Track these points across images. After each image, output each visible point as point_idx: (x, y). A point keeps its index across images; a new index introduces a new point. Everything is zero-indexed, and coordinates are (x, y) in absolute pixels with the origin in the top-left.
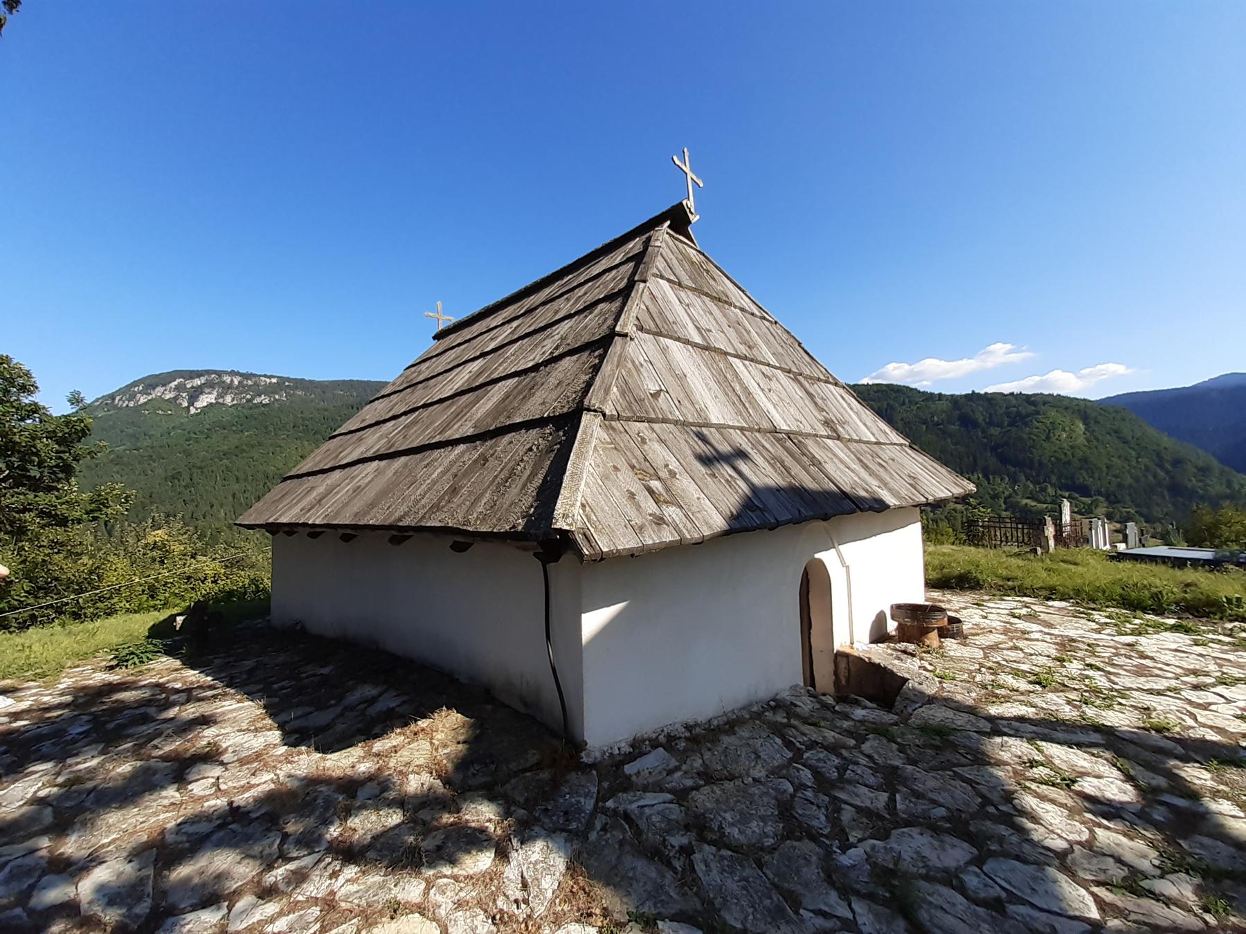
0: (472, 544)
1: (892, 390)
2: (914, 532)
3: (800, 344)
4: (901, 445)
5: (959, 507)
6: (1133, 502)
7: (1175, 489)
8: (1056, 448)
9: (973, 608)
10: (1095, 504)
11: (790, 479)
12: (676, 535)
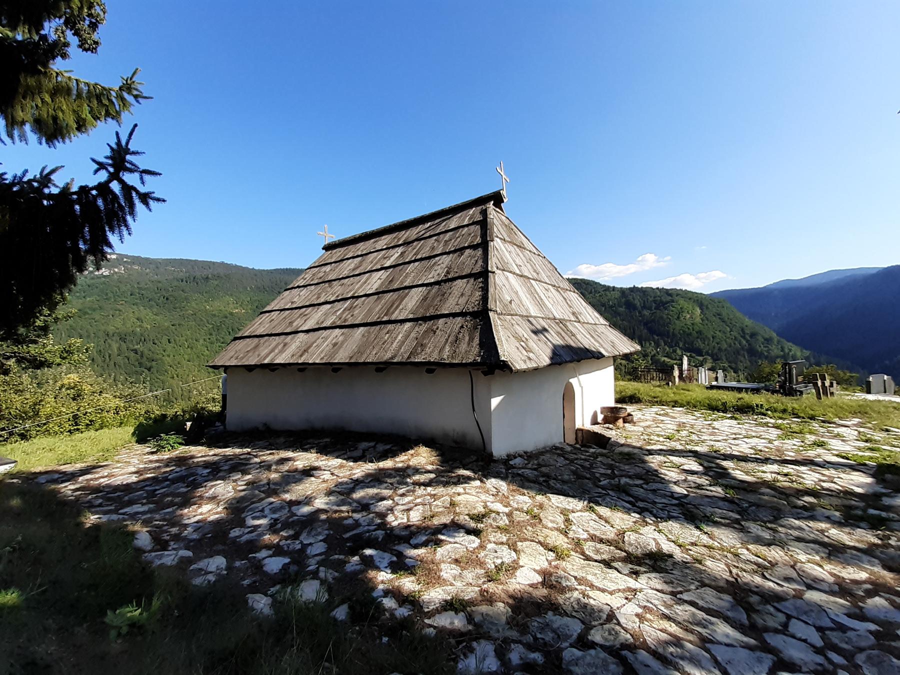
0: (435, 370)
2: (610, 371)
3: (556, 269)
4: (605, 325)
5: (624, 362)
6: (727, 360)
7: (752, 352)
8: (683, 324)
10: (705, 361)
11: (565, 342)
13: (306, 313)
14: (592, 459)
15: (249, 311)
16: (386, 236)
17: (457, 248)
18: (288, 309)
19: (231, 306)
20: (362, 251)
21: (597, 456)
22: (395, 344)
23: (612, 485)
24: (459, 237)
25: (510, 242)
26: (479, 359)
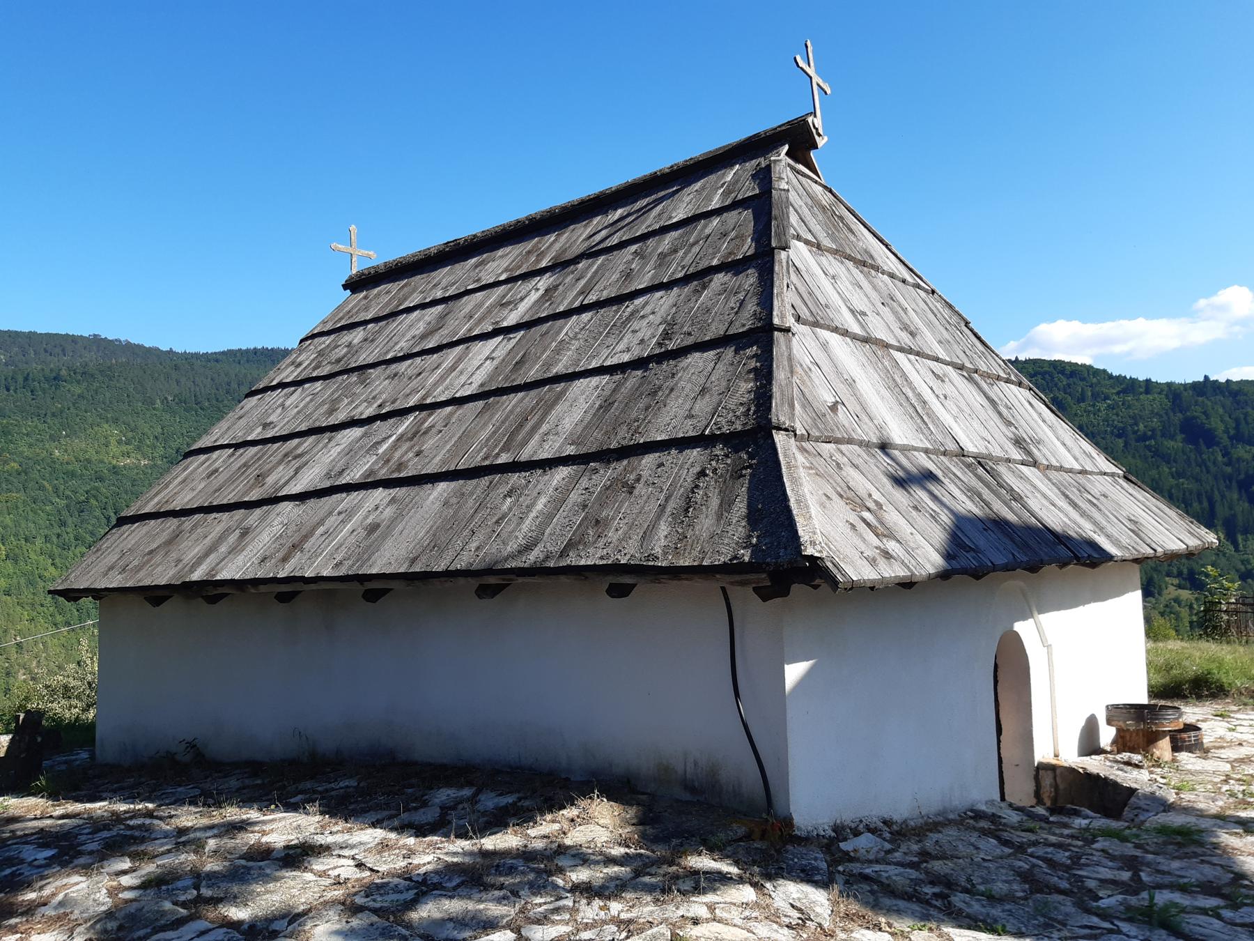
0: (634, 586)
1: (1062, 372)
2: (1131, 604)
3: (967, 324)
4: (1113, 475)
9: (1216, 720)
12: (906, 570)
13: (299, 451)
14: (1080, 843)
15: (159, 462)
16: (510, 248)
17: (691, 270)
18: (253, 443)
19: (114, 449)
20: (445, 289)
21: (1095, 836)
22: (528, 522)
23: (1129, 908)
24: (696, 243)
25: (835, 252)
26: (746, 555)
